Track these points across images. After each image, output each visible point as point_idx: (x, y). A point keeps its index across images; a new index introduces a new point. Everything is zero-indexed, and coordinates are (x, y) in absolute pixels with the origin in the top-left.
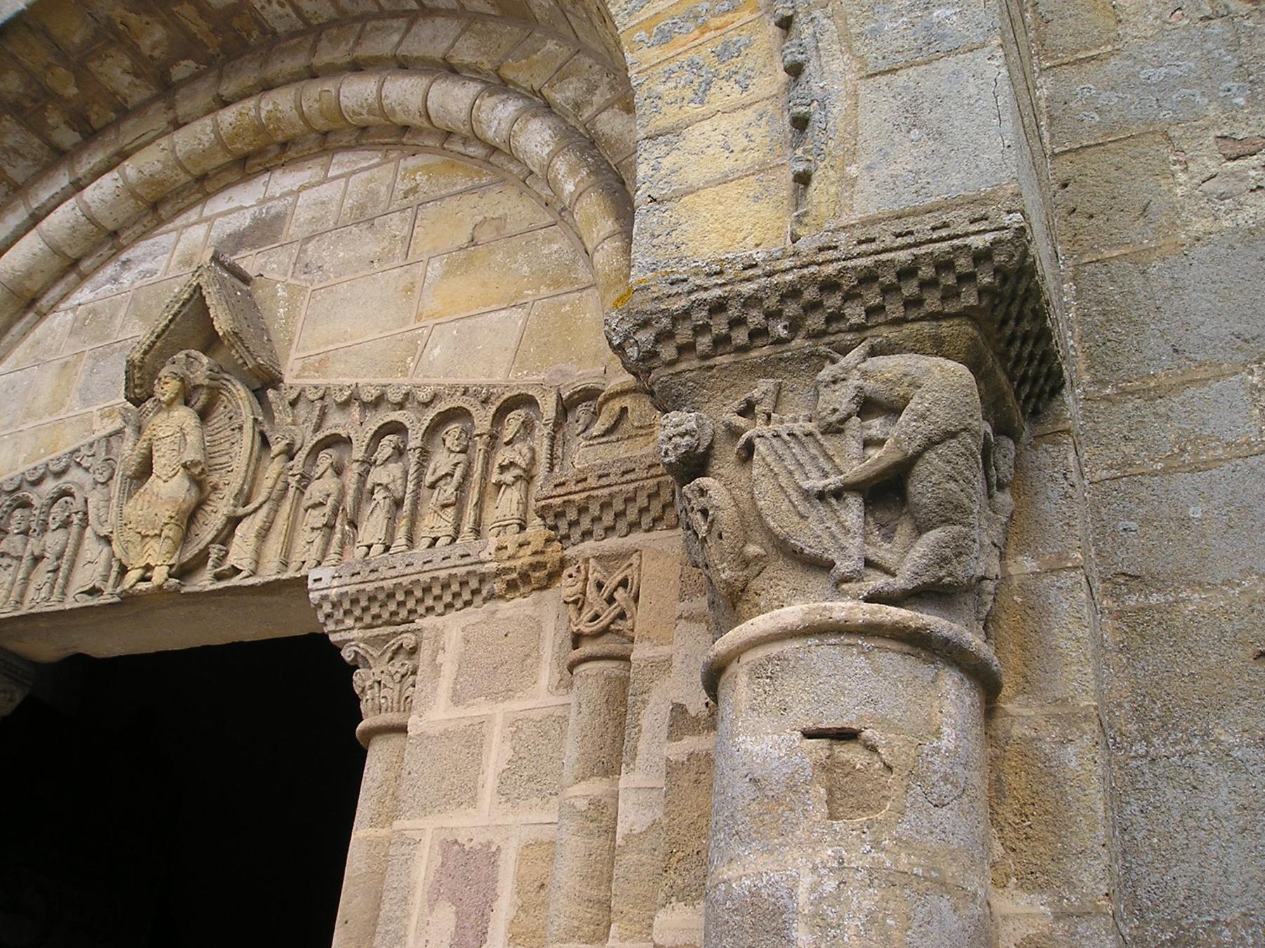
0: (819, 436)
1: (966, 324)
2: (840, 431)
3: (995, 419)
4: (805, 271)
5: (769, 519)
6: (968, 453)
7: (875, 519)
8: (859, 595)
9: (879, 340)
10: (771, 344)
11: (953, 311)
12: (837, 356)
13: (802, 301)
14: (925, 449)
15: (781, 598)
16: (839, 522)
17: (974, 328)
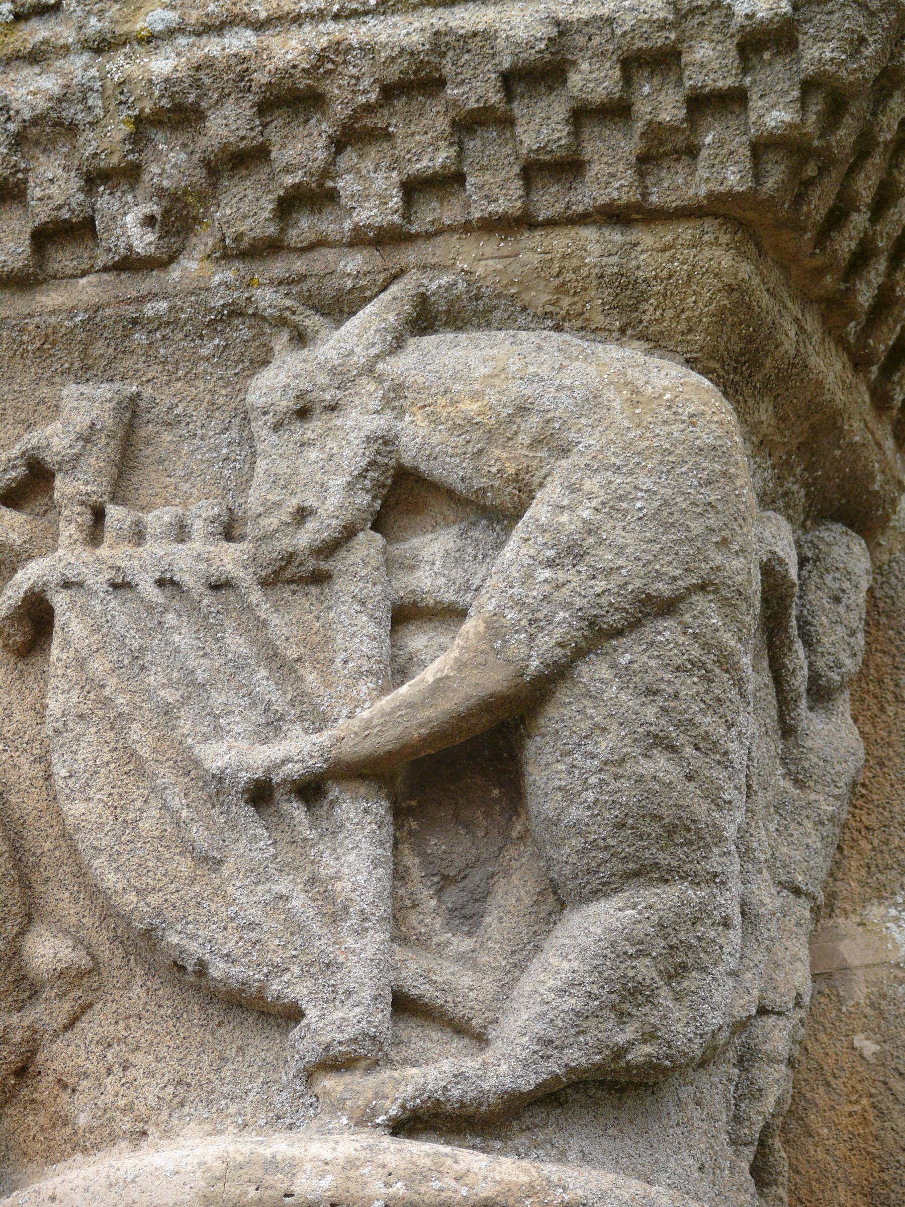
0: (256, 596)
1: (716, 243)
2: (320, 578)
3: (807, 485)
4: (213, 47)
5: (99, 862)
6: (709, 660)
7: (427, 861)
8: (375, 1112)
9: (445, 280)
10: (106, 269)
11: (673, 201)
12: (312, 321)
13: (203, 142)
14: (580, 653)
15: (140, 1107)
16: (313, 880)
17: (741, 254)
